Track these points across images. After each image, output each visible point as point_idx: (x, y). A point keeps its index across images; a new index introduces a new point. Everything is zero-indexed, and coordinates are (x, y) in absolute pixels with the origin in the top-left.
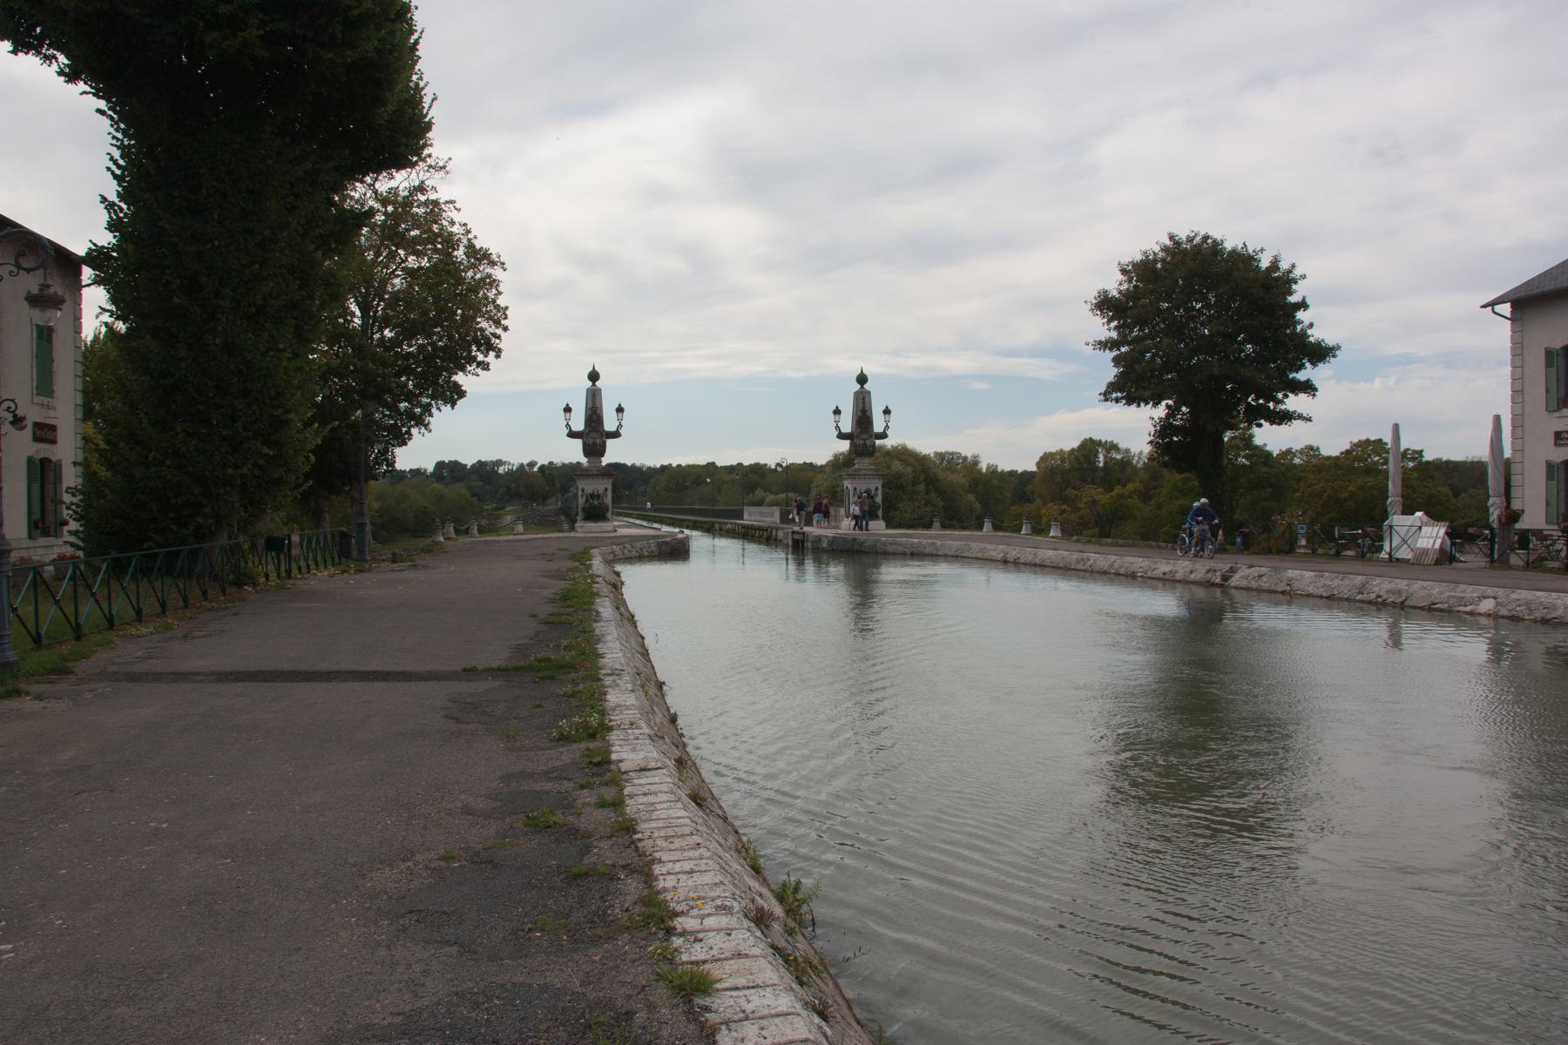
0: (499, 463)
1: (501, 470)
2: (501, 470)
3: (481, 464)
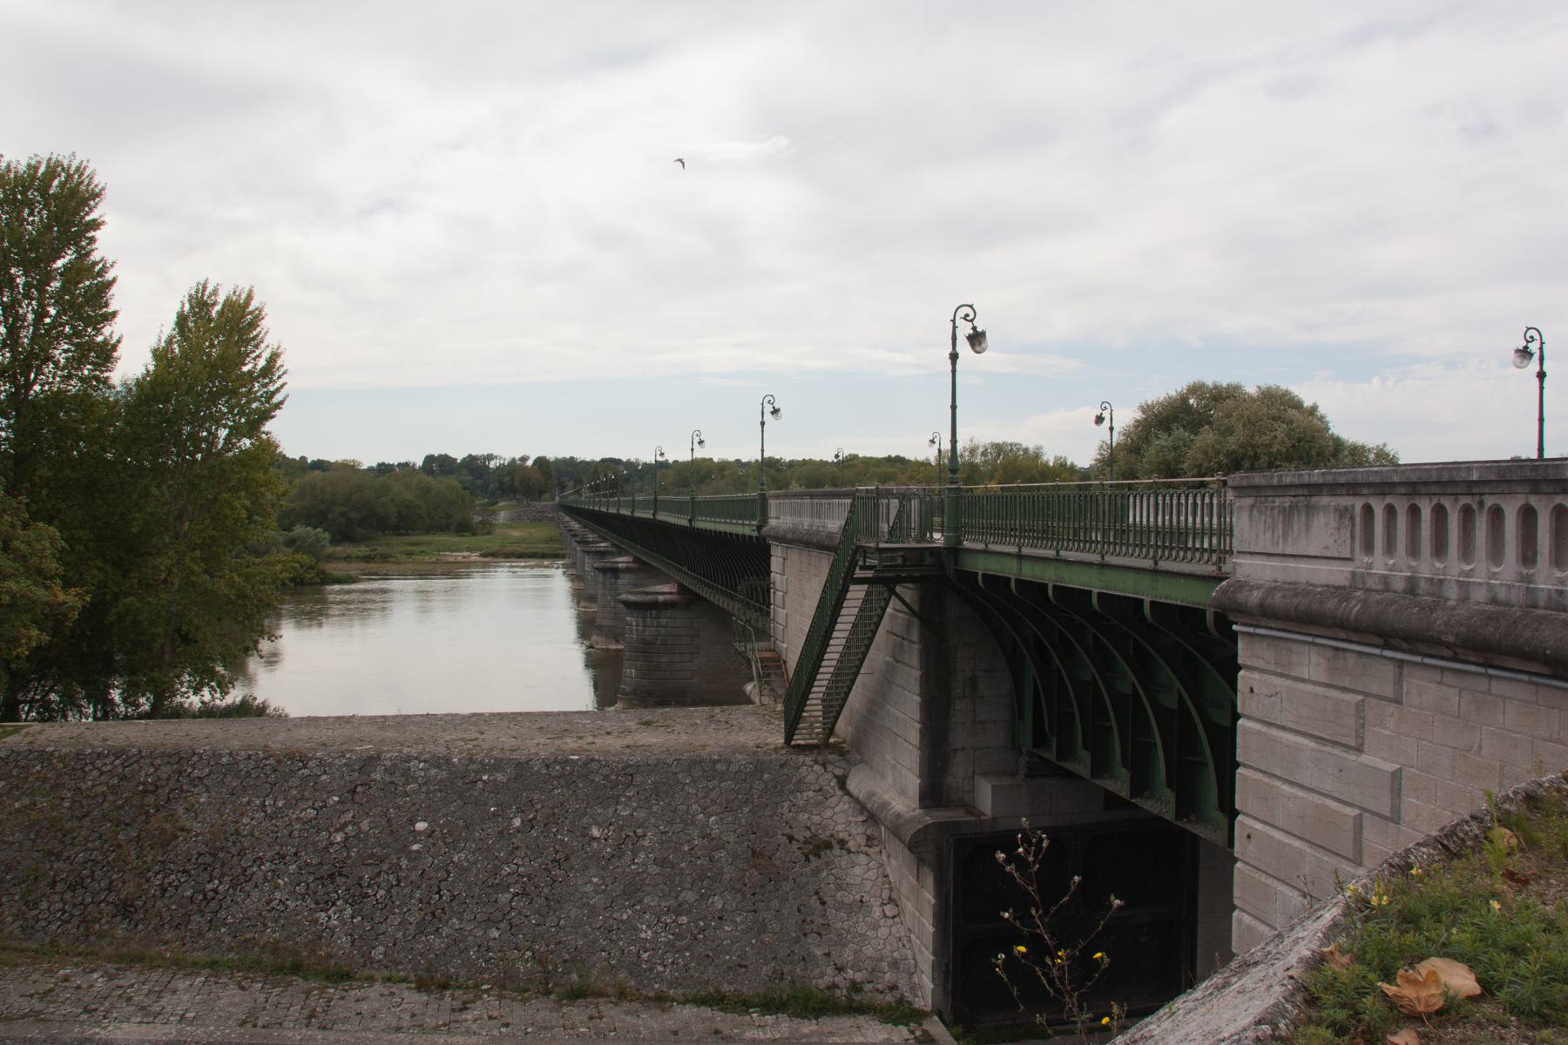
0: (490, 457)
1: (492, 464)
2: (492, 464)
3: (471, 459)
